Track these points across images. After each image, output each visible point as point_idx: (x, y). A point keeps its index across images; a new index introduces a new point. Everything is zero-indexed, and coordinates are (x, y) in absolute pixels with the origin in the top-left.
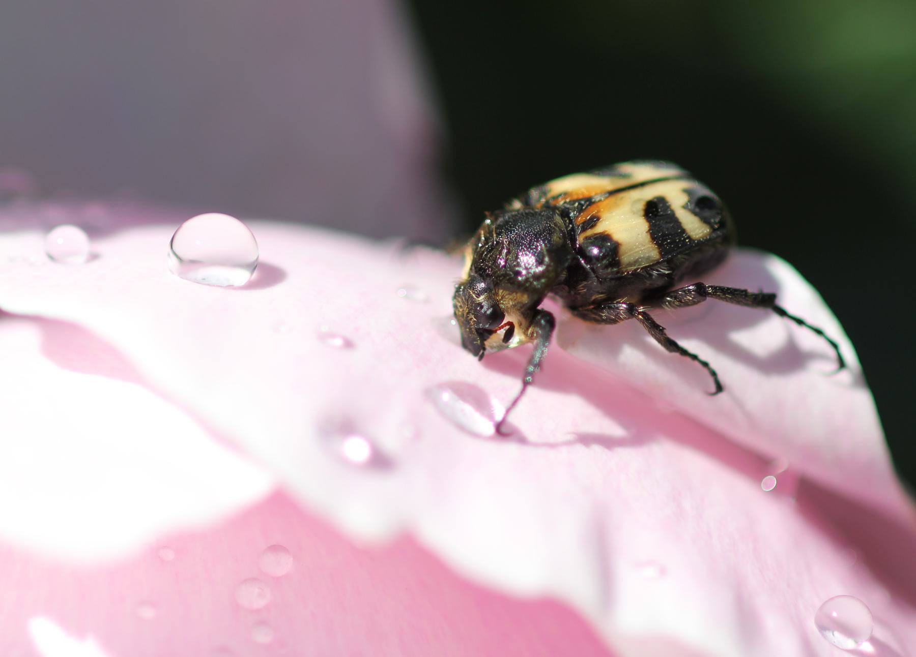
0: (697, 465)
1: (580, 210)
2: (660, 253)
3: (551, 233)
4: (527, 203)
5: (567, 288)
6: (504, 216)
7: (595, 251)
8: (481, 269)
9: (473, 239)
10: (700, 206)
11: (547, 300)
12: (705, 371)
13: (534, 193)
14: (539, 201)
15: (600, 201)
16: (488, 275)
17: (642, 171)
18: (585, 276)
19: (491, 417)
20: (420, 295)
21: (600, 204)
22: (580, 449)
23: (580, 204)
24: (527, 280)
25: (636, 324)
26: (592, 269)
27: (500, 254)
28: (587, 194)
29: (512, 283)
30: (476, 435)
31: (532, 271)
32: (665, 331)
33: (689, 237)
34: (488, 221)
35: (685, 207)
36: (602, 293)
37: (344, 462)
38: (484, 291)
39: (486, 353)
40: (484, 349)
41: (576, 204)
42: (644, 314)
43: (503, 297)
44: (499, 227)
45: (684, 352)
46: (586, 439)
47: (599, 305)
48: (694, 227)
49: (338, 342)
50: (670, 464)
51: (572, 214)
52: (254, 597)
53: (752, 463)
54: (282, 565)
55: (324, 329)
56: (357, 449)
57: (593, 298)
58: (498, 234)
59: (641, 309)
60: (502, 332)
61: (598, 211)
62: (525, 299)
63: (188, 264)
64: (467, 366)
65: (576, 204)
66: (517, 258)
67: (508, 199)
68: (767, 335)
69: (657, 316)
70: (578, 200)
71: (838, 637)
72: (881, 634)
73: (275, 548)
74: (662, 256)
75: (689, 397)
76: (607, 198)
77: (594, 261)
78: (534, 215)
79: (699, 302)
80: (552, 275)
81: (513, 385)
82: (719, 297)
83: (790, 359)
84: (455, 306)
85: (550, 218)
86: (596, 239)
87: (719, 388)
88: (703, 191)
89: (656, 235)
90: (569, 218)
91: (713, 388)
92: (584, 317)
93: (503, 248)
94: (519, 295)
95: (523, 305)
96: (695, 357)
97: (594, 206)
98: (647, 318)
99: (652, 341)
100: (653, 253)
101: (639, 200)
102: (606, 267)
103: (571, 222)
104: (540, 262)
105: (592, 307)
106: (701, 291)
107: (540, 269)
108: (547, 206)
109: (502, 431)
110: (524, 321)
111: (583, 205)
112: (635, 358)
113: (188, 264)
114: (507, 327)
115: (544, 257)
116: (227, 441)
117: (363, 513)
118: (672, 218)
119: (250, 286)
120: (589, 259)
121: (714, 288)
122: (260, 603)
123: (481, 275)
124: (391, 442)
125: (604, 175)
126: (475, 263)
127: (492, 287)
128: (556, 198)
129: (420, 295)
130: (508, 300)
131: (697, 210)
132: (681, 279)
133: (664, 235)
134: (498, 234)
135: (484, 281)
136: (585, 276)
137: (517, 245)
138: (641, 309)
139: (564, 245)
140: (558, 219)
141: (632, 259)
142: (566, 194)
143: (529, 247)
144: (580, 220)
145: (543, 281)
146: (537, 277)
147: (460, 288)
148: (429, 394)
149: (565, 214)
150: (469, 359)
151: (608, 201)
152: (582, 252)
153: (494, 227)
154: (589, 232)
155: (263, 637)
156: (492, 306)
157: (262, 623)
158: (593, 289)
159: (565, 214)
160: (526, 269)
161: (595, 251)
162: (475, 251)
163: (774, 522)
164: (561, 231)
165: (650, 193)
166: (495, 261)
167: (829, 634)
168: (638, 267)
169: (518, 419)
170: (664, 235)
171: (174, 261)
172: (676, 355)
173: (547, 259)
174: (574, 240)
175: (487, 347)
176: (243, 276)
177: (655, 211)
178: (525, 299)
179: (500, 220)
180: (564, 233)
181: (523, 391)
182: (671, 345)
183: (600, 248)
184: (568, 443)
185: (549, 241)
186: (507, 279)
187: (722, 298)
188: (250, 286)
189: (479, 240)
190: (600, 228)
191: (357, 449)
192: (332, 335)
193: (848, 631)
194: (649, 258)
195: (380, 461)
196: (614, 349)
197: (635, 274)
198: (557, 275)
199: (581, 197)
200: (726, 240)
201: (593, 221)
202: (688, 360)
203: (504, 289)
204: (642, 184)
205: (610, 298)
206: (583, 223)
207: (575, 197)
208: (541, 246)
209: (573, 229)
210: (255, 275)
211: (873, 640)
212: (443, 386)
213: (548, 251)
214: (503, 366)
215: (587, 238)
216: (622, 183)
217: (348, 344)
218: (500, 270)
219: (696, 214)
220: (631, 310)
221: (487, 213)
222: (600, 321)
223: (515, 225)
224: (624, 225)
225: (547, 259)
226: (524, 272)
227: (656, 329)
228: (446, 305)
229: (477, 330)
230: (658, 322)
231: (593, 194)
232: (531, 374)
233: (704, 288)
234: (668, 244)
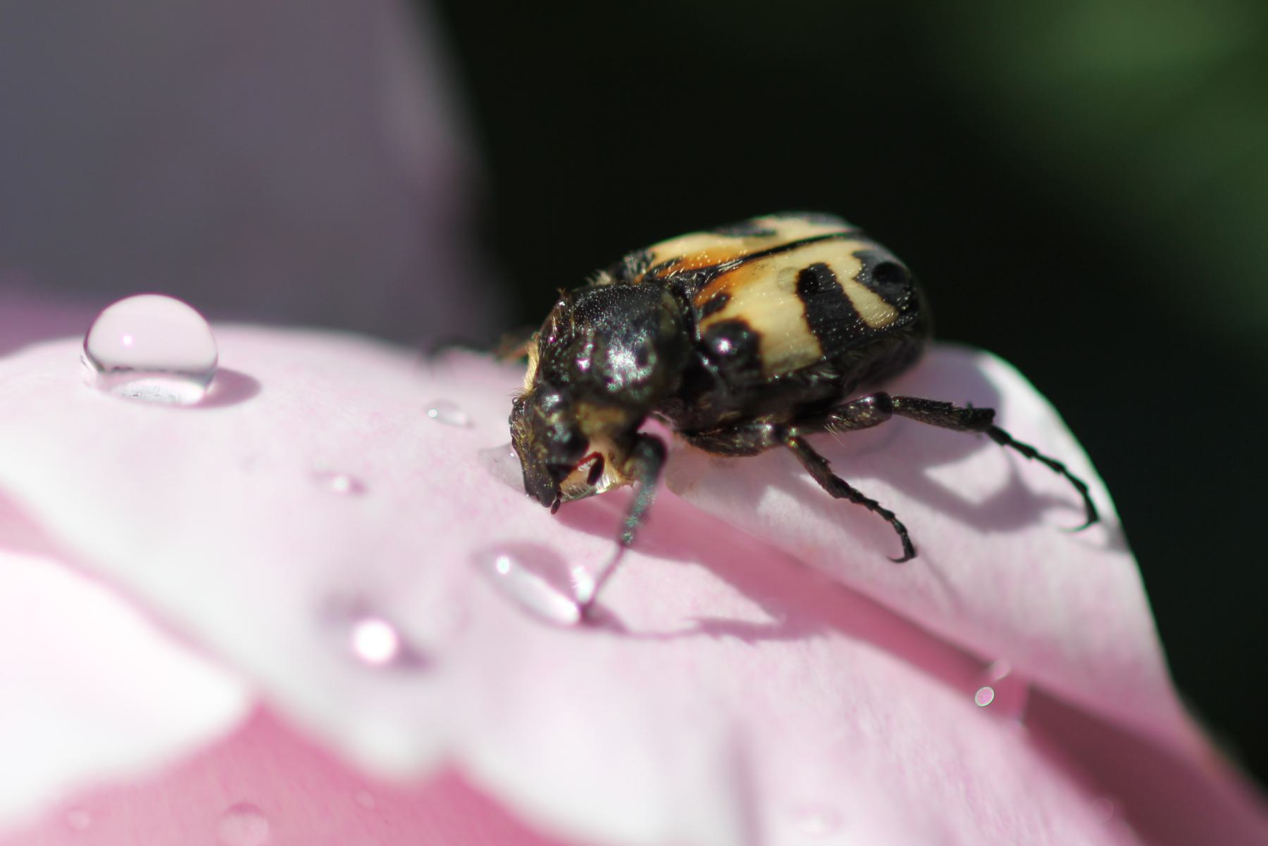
1: (702, 284)
5: (681, 402)
7: (724, 346)
10: (879, 277)
11: (652, 424)
12: (889, 525)
13: (631, 261)
16: (564, 384)
17: (792, 228)
21: (729, 275)
22: (706, 643)
23: (699, 276)
25: (787, 455)
26: (721, 373)
27: (582, 349)
30: (548, 622)
33: (864, 324)
36: (735, 409)
37: (358, 664)
38: (557, 407)
43: (586, 417)
44: (578, 311)
45: (857, 497)
46: (714, 628)
47: (729, 428)
48: (872, 308)
49: (341, 484)
51: (688, 292)
53: (959, 666)
56: (375, 641)
57: (722, 416)
58: (579, 322)
60: (585, 469)
61: (728, 287)
63: (112, 371)
64: (535, 520)
68: (979, 472)
69: (818, 443)
70: (697, 270)
81: (603, 548)
83: (1014, 509)
84: (513, 431)
85: (656, 297)
90: (684, 296)
92: (707, 446)
93: (586, 343)
96: (873, 505)
97: (722, 278)
99: (811, 481)
101: (789, 269)
103: (687, 302)
104: (641, 361)
108: (650, 277)
109: (591, 616)
110: (618, 453)
111: (704, 278)
112: (785, 509)
113: (112, 371)
114: (593, 461)
117: (387, 736)
119: (207, 403)
120: (716, 357)
121: (904, 401)
124: (427, 625)
125: (728, 234)
128: (660, 267)
129: (460, 418)
131: (876, 283)
140: (668, 298)
143: (626, 339)
146: (637, 385)
148: (481, 560)
149: (678, 290)
152: (706, 348)
154: (716, 318)
158: (720, 404)
159: (678, 290)
161: (724, 346)
166: (574, 361)
170: (827, 322)
173: (653, 359)
174: (692, 330)
176: (193, 392)
177: (813, 284)
182: (838, 487)
183: (732, 340)
184: (687, 633)
185: (657, 331)
186: (592, 388)
187: (915, 417)
188: (207, 403)
189: (549, 331)
190: (732, 311)
191: (375, 641)
192: (329, 475)
195: (410, 659)
196: (752, 494)
197: (784, 379)
201: (721, 302)
204: (793, 246)
205: (747, 417)
208: (643, 338)
209: (691, 314)
210: (212, 388)
215: (712, 327)
216: (763, 245)
217: (357, 488)
219: (874, 290)
220: (779, 435)
222: (732, 451)
223: (603, 309)
224: (767, 306)
226: (618, 378)
227: (816, 464)
228: (501, 433)
230: (820, 450)
232: (632, 531)
233: (889, 400)
234: (833, 334)
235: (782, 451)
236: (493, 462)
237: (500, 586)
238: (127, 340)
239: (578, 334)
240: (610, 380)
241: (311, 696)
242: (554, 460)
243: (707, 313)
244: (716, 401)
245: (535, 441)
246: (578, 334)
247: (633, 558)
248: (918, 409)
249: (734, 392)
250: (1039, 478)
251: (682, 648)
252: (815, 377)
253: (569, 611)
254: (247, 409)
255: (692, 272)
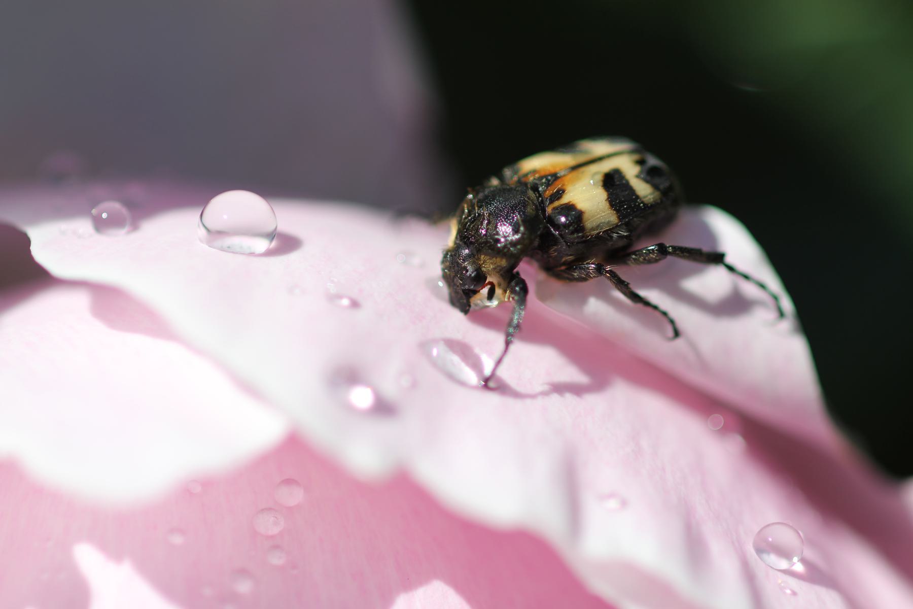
0: (654, 407)
1: (548, 184)
2: (618, 217)
3: (525, 206)
4: (501, 178)
5: (540, 252)
6: (483, 191)
7: (563, 219)
8: (465, 237)
9: (458, 213)
10: (650, 175)
11: (515, 261)
13: (507, 172)
14: (512, 177)
15: (564, 176)
16: (471, 243)
17: (599, 147)
18: (554, 241)
19: (476, 365)
20: (416, 261)
22: (555, 397)
24: (505, 246)
25: (605, 281)
26: (560, 235)
27: (482, 224)
28: (552, 170)
29: (493, 250)
30: (463, 384)
31: (509, 239)
32: (631, 286)
33: (642, 202)
34: (470, 196)
35: (638, 176)
37: (350, 409)
39: (471, 309)
40: (470, 306)
41: (544, 180)
42: (611, 272)
44: (480, 201)
46: (559, 388)
47: (571, 266)
48: (643, 190)
49: (345, 302)
50: (627, 407)
51: (540, 189)
52: (269, 525)
53: (702, 401)
54: (294, 497)
55: (333, 290)
56: (362, 397)
57: (564, 260)
58: (479, 207)
59: (608, 268)
60: (485, 291)
61: (563, 185)
62: (504, 263)
63: (215, 234)
64: (455, 322)
65: (544, 180)
66: (496, 227)
67: (487, 177)
68: (711, 283)
69: (623, 272)
70: (546, 176)
71: (772, 559)
72: (809, 554)
73: (288, 482)
74: (620, 220)
75: (650, 342)
76: (570, 172)
77: (562, 228)
78: (510, 190)
79: (660, 259)
80: (527, 242)
81: (497, 339)
82: (678, 255)
83: (735, 305)
84: (443, 270)
85: (524, 193)
86: (562, 209)
87: (677, 333)
88: (652, 161)
89: (613, 202)
90: (538, 192)
91: (670, 333)
92: (558, 276)
93: (484, 219)
94: (498, 259)
95: (502, 269)
96: (655, 308)
98: (613, 275)
99: (618, 295)
100: (611, 217)
101: (596, 173)
102: (572, 233)
103: (540, 196)
104: (516, 231)
105: (563, 268)
106: (663, 250)
107: (517, 237)
108: (520, 182)
109: (490, 383)
110: (502, 282)
112: (601, 310)
113: (215, 234)
114: (489, 286)
115: (519, 227)
116: (250, 389)
117: (365, 454)
118: (627, 187)
119: (269, 253)
120: (557, 226)
121: (674, 247)
122: (275, 531)
123: (465, 243)
124: (391, 389)
126: (460, 232)
127: (475, 252)
128: (526, 175)
130: (489, 265)
131: (648, 178)
132: (639, 237)
133: (621, 202)
134: (479, 207)
135: (468, 247)
136: (554, 241)
137: (495, 217)
138: (608, 268)
139: (537, 216)
140: (531, 193)
141: (594, 224)
142: (534, 172)
143: (506, 218)
144: (548, 193)
145: (519, 247)
146: (514, 244)
147: (447, 254)
148: (424, 346)
149: (535, 188)
150: (457, 315)
151: (570, 176)
152: (551, 221)
153: (475, 201)
154: (556, 204)
155: (277, 560)
156: (476, 270)
157: (276, 547)
158: (563, 252)
160: (505, 237)
162: (460, 222)
163: (720, 456)
164: (534, 204)
165: (606, 166)
166: (477, 230)
167: (765, 556)
168: (601, 231)
169: (504, 373)
170: (621, 202)
171: (202, 232)
172: (640, 306)
173: (522, 229)
174: (544, 211)
175: (472, 304)
176: (262, 245)
177: (613, 182)
178: (504, 263)
179: (481, 196)
180: (536, 206)
181: (508, 344)
182: (636, 298)
183: (566, 217)
184: (544, 394)
185: (524, 213)
186: (489, 246)
187: (680, 257)
188: (269, 253)
190: (565, 200)
191: (362, 397)
192: (340, 297)
193: (785, 554)
194: (609, 222)
195: (383, 408)
196: (583, 301)
197: (598, 236)
198: (531, 242)
199: (547, 173)
200: (676, 203)
201: (559, 194)
202: (649, 310)
203: (486, 255)
204: (600, 159)
205: (581, 259)
206: (551, 196)
207: (543, 173)
208: (517, 217)
210: (274, 244)
211: (803, 561)
212: (435, 341)
213: (523, 221)
214: (485, 319)
215: (554, 209)
216: (582, 159)
217: (355, 304)
218: (481, 238)
219: (647, 181)
220: (599, 270)
221: (469, 189)
222: (572, 279)
223: (494, 200)
224: (586, 196)
225: (522, 229)
226: (502, 240)
227: (622, 285)
228: (436, 269)
229: (464, 291)
230: (623, 278)
231: (557, 170)
232: (513, 332)
233: (666, 247)
235: (602, 278)
236: (435, 289)
237: (434, 363)
238: (225, 217)
239: (479, 215)
240: (498, 241)
241: (321, 429)
242: (467, 287)
243: (552, 202)
244: (562, 249)
245: (454, 277)
246: (479, 215)
247: (519, 348)
248: (682, 252)
249: (570, 245)
250: (750, 290)
251: (540, 401)
252: (615, 235)
253: (472, 378)
254: (294, 257)
255: (541, 178)
